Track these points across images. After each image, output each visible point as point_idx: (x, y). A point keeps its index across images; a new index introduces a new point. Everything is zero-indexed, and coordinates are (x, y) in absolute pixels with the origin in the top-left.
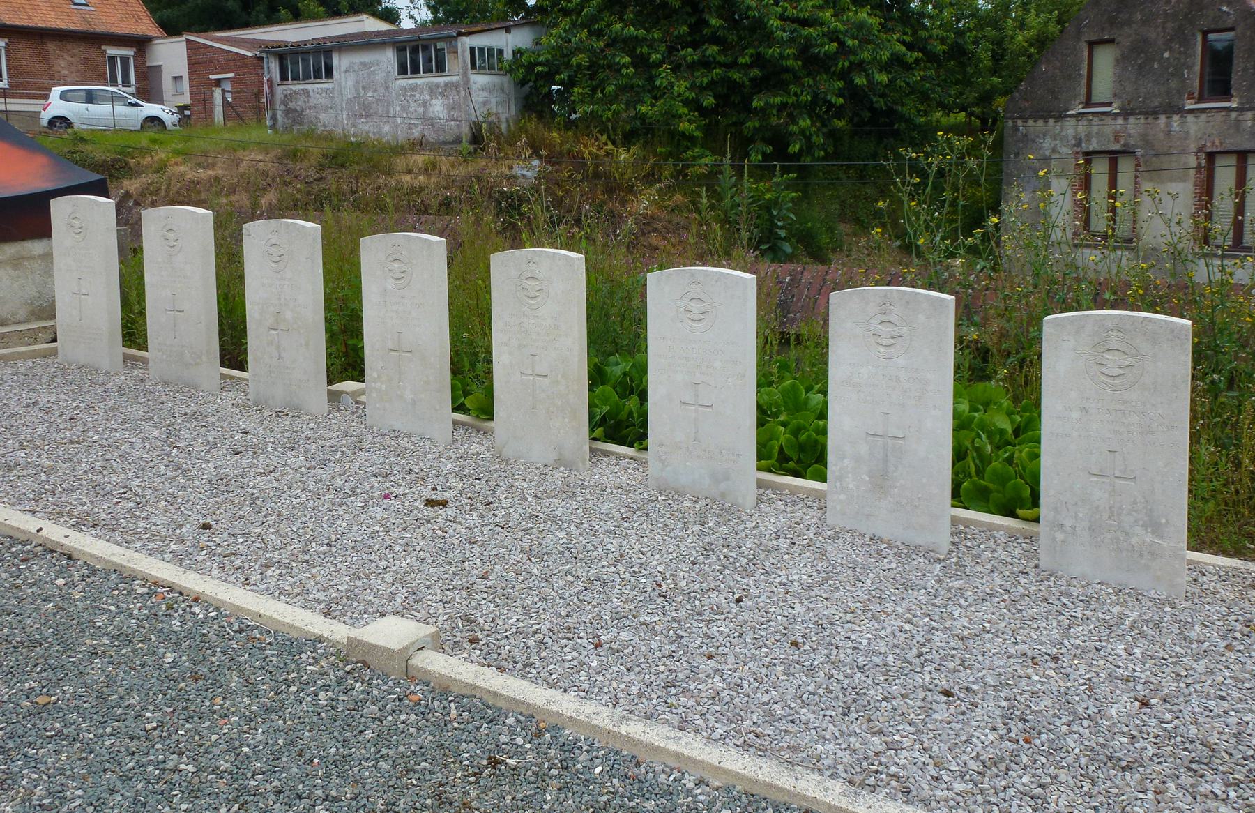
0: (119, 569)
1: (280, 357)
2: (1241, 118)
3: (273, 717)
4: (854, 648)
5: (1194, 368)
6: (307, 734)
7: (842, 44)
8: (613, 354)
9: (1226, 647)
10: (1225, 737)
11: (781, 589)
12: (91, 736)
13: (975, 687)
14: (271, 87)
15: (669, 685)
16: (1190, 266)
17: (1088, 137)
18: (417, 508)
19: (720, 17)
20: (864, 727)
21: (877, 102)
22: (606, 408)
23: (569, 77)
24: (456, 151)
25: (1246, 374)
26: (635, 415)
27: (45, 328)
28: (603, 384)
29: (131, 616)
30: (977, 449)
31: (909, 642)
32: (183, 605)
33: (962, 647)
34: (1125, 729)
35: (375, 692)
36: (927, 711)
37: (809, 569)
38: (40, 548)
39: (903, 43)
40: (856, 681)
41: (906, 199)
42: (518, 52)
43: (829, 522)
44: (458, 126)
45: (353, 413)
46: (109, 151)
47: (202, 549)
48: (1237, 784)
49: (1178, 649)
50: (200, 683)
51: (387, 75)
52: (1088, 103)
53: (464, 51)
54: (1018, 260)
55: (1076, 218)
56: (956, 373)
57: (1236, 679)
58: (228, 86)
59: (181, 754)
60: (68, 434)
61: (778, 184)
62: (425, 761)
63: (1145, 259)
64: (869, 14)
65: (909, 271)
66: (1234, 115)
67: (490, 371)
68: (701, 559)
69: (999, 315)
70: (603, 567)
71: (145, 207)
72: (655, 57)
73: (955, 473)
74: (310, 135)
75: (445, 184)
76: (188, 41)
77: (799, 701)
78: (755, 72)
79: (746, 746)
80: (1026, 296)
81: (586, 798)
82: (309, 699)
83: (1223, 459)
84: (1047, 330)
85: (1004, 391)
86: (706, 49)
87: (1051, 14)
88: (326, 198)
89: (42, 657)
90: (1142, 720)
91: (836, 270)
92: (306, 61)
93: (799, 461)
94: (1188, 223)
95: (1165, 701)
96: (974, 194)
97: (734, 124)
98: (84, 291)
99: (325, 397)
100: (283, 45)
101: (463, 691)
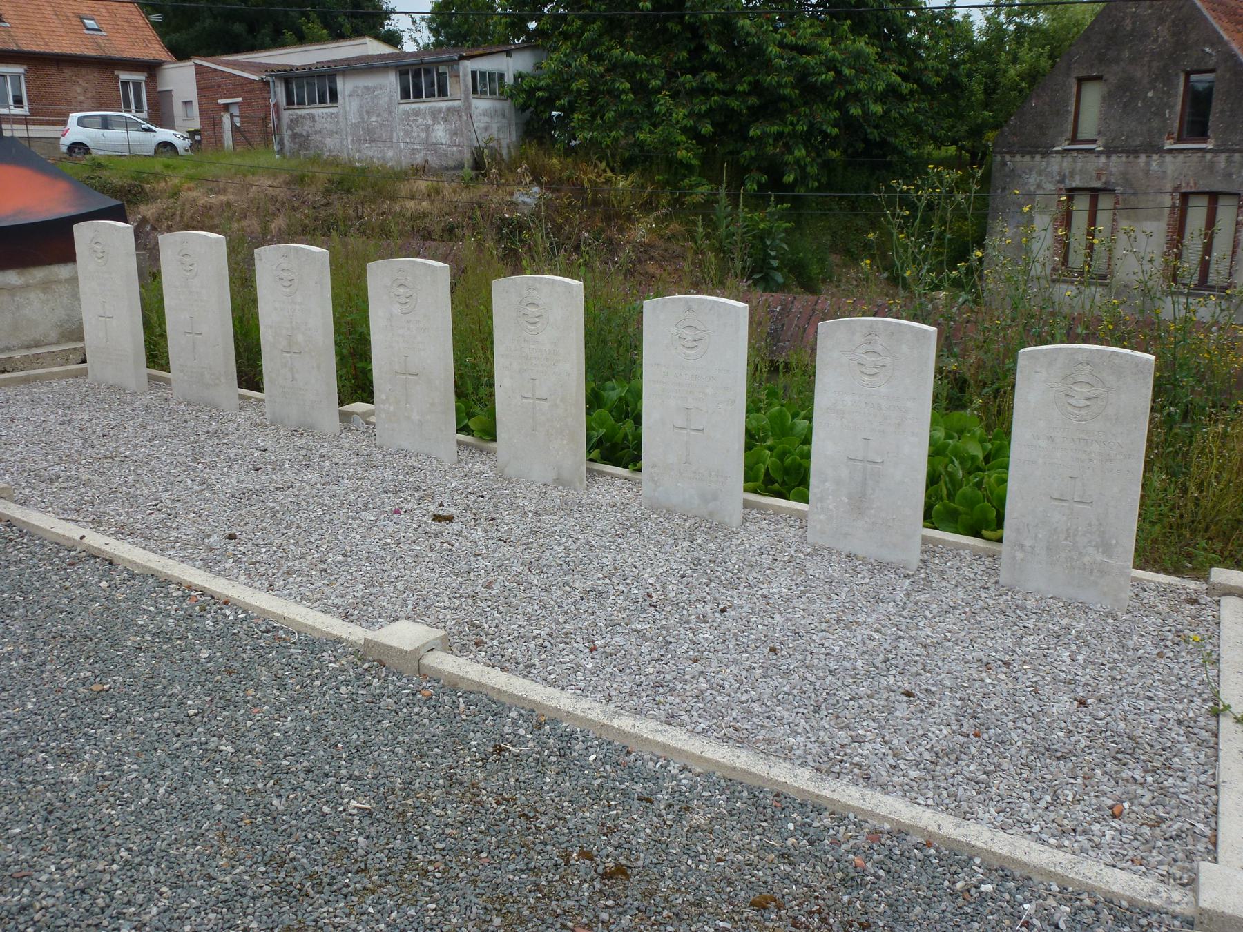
0: (155, 574)
1: (294, 379)
2: (1215, 159)
3: (300, 707)
4: (827, 654)
5: (1154, 401)
6: (331, 722)
7: (839, 73)
8: (609, 379)
9: (1158, 654)
10: (1148, 732)
11: (762, 601)
12: (141, 719)
13: (934, 689)
14: (277, 112)
15: (657, 685)
16: (1158, 302)
17: (1072, 174)
18: (425, 523)
19: (720, 43)
20: (832, 723)
21: (871, 133)
22: (602, 431)
23: (569, 102)
24: (458, 176)
25: (1200, 407)
26: (630, 438)
27: (75, 349)
28: (600, 407)
29: (169, 616)
30: (950, 474)
31: (877, 649)
32: (215, 608)
33: (925, 653)
34: (1063, 725)
35: (391, 687)
36: (890, 709)
37: (789, 583)
38: (84, 554)
39: (899, 73)
40: (828, 683)
41: (895, 231)
42: (519, 77)
43: (809, 540)
44: (460, 152)
45: (363, 433)
46: (125, 177)
47: (229, 557)
48: (1154, 771)
49: (1116, 656)
50: (234, 676)
51: (391, 100)
52: (1074, 140)
53: (465, 75)
54: (999, 293)
55: (1055, 254)
56: (934, 401)
57: (1164, 682)
58: (236, 111)
59: (221, 737)
60: (102, 450)
61: (772, 214)
62: (438, 747)
63: (1117, 296)
64: (866, 44)
65: (895, 302)
66: (1209, 156)
67: (492, 395)
68: (689, 572)
69: (978, 347)
70: (599, 579)
71: (162, 232)
72: (654, 83)
73: (928, 496)
74: (316, 159)
75: (447, 209)
76: (196, 65)
77: (775, 700)
78: (753, 100)
79: (726, 739)
80: (1005, 329)
81: (582, 781)
82: (332, 692)
83: (1172, 486)
84: (1021, 362)
85: (978, 419)
86: (705, 76)
87: (1043, 49)
88: (332, 224)
89: (93, 650)
90: (1079, 718)
91: (825, 301)
92: (311, 85)
93: (783, 483)
94: (1159, 261)
95: (1100, 701)
96: (960, 228)
97: (731, 153)
98: (108, 314)
99: (146, 379)
100: (288, 69)
101: (471, 688)
